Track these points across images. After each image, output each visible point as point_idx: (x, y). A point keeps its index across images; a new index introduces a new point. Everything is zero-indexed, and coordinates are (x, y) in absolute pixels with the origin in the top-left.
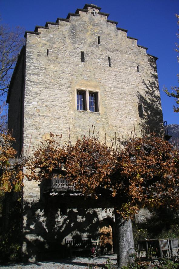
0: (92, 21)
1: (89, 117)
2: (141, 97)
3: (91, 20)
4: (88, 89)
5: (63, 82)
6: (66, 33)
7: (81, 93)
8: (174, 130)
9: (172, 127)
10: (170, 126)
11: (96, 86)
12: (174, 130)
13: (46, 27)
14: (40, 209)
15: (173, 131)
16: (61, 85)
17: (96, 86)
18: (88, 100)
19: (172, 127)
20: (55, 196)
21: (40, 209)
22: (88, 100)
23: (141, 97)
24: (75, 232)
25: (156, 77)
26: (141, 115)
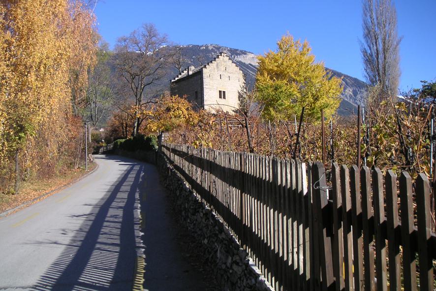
0: (348, 235)
1: (222, 101)
2: (239, 93)
3: (223, 59)
4: (222, 90)
5: (214, 87)
6: (215, 67)
7: (220, 92)
8: (213, 53)
9: (210, 48)
10: (207, 47)
11: (225, 89)
12: (213, 53)
13: (208, 64)
14: (417, 230)
15: (212, 56)
16: (214, 89)
17: (225, 89)
18: (222, 94)
19: (210, 48)
20: (388, 241)
21: (417, 230)
22: (222, 94)
23: (239, 93)
24: (142, 245)
25: (245, 83)
26: (239, 100)
